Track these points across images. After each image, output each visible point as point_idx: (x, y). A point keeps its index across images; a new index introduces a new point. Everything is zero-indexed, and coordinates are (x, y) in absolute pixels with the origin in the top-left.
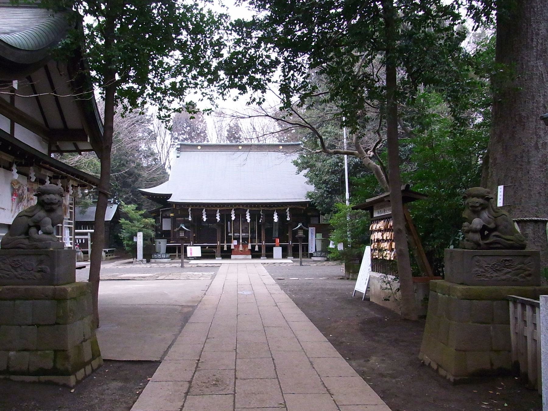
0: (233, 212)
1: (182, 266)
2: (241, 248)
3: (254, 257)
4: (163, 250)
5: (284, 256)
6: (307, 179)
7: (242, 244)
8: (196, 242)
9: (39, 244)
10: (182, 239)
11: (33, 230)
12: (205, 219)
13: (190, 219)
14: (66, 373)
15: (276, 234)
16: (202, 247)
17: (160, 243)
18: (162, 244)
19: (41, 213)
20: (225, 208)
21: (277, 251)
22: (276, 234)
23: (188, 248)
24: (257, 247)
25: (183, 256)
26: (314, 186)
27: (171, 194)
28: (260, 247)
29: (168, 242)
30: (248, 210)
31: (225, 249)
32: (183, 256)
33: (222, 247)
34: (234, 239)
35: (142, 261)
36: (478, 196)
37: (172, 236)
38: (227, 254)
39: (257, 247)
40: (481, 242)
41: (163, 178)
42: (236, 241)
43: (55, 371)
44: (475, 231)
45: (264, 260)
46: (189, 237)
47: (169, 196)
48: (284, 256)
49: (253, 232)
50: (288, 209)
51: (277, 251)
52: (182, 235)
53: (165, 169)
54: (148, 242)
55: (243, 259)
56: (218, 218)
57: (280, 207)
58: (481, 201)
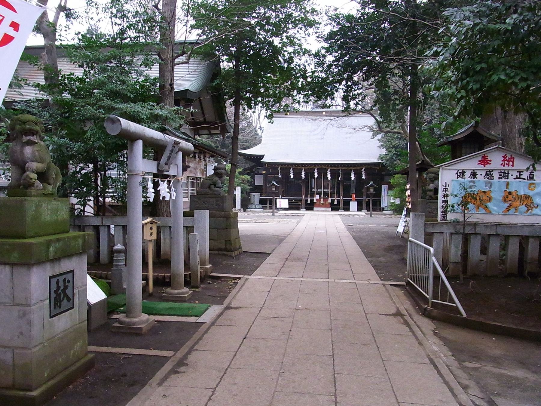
0: (316, 171)
1: (273, 215)
2: (322, 202)
3: (333, 210)
4: (257, 201)
5: (359, 209)
6: (379, 144)
7: (323, 198)
8: (285, 195)
9: (216, 193)
10: (273, 192)
11: (213, 186)
12: (292, 177)
13: (280, 177)
14: (231, 250)
15: (353, 190)
16: (289, 200)
17: (254, 196)
18: (256, 197)
19: (216, 179)
20: (310, 168)
21: (353, 205)
22: (353, 190)
23: (278, 200)
24: (336, 201)
25: (274, 207)
26: (385, 149)
27: (264, 155)
28: (338, 201)
29: (261, 195)
30: (329, 170)
31: (309, 202)
32: (274, 207)
33: (306, 201)
34: (317, 194)
35: (240, 210)
36: (432, 173)
37: (264, 191)
38: (310, 207)
39: (336, 201)
40: (433, 196)
41: (256, 141)
42: (318, 196)
43: (226, 250)
44: (430, 191)
45: (341, 212)
46: (279, 192)
47: (263, 156)
48: (359, 209)
49: (333, 188)
50: (364, 169)
51: (353, 205)
52: (273, 189)
53: (256, 131)
54: (245, 195)
55: (324, 211)
56: (303, 176)
57: (357, 167)
58: (434, 175)
